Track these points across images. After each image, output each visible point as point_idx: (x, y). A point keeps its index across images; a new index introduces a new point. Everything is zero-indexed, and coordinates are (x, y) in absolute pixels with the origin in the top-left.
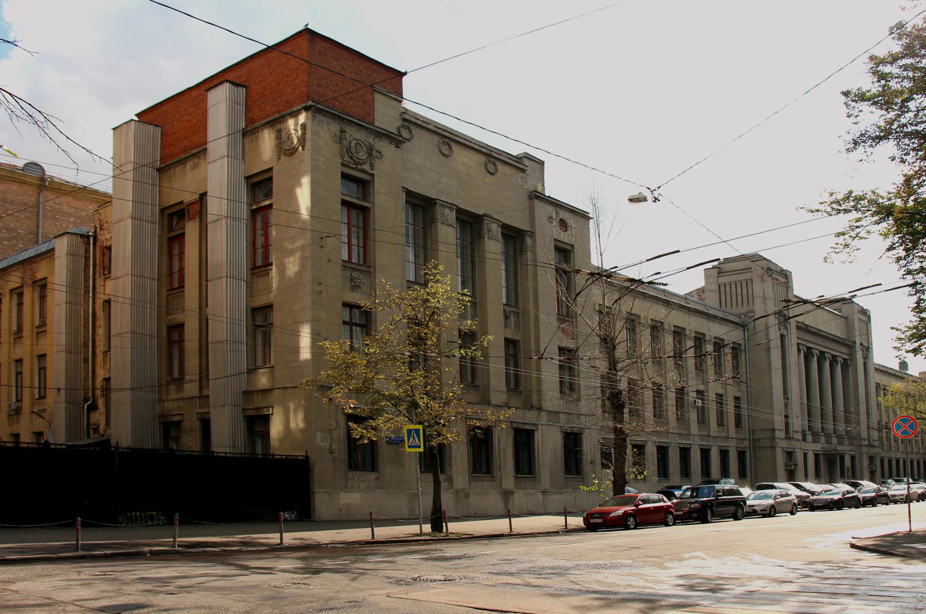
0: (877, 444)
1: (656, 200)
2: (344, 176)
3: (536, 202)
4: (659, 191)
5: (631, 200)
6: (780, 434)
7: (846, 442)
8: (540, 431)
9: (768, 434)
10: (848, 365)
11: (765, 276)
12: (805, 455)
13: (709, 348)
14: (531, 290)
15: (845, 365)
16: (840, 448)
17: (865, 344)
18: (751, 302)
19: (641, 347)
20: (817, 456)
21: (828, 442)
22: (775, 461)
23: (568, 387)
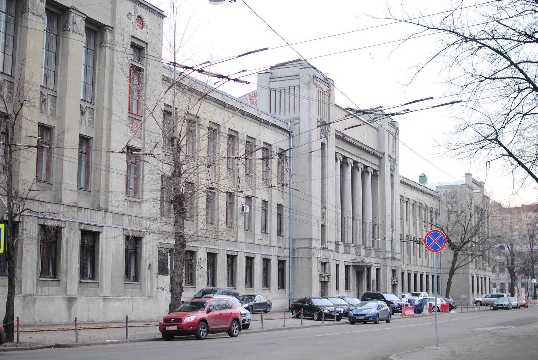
0: (399, 257)
2: (336, 146)
6: (316, 244)
7: (373, 253)
9: (306, 244)
11: (312, 84)
15: (375, 176)
16: (367, 260)
17: (393, 156)
18: (297, 109)
20: (347, 267)
21: (358, 254)
23: (133, 189)
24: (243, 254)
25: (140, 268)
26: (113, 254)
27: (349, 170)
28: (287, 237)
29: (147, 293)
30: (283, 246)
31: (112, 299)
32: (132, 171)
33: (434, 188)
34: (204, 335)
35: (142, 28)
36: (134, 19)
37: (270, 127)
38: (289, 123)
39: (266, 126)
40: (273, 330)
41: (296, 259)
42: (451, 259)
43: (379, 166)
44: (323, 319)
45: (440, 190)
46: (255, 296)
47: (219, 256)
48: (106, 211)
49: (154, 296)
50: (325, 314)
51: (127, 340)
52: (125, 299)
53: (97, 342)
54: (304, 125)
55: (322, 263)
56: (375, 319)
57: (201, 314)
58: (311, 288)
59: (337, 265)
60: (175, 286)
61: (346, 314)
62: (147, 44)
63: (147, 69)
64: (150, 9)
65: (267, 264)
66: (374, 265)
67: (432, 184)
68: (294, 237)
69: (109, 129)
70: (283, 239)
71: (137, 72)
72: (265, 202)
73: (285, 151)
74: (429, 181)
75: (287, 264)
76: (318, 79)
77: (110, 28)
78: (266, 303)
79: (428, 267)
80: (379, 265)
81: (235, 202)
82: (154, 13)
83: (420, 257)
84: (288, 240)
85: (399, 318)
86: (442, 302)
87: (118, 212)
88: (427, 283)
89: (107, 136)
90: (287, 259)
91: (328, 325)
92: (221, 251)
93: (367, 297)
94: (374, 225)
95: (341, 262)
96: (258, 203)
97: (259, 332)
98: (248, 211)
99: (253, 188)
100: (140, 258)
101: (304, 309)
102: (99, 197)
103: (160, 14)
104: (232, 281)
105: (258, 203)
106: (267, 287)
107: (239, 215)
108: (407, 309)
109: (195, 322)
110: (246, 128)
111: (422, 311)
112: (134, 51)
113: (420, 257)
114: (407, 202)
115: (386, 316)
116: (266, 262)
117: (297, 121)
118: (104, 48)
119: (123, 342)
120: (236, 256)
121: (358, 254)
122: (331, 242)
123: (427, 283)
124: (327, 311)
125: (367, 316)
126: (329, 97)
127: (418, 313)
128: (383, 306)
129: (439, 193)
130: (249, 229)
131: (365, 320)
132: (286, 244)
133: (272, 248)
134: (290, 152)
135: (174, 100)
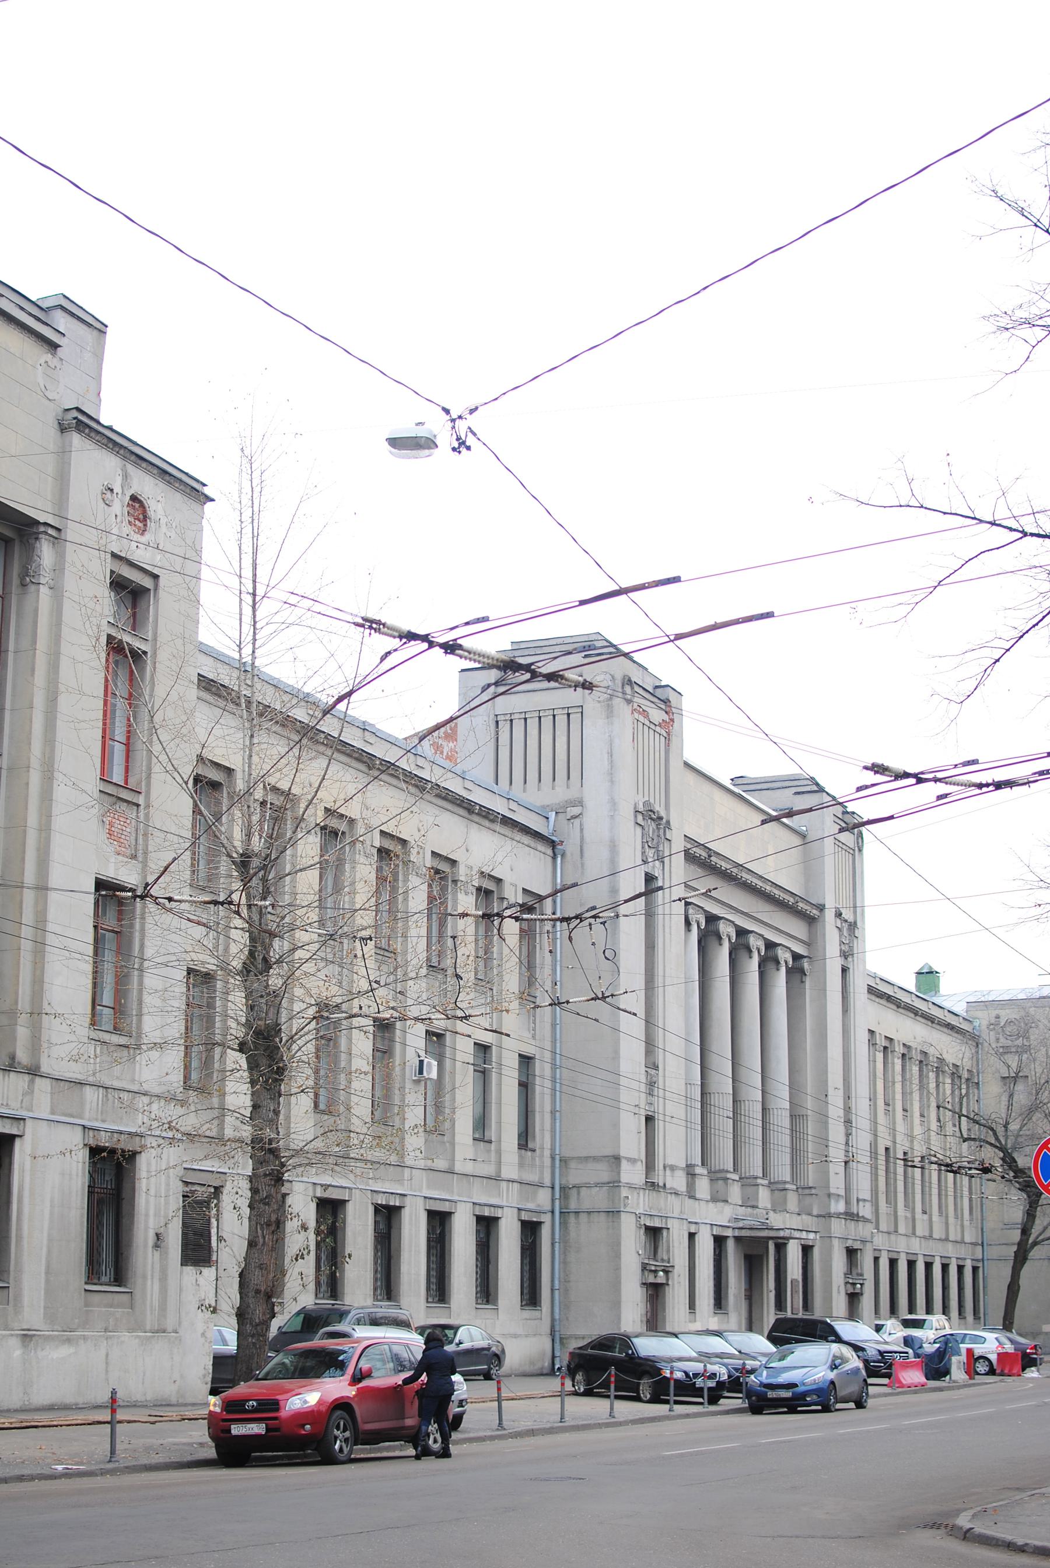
0: (866, 1211)
1: (461, 445)
3: (76, 439)
4: (472, 421)
5: (395, 443)
6: (632, 1174)
7: (792, 1201)
8: (28, 1137)
9: (602, 1173)
10: (803, 972)
11: (618, 702)
12: (876, 1259)
13: (466, 902)
14: (39, 700)
15: (796, 972)
16: (777, 1220)
17: (847, 915)
18: (575, 774)
19: (353, 893)
20: (719, 1241)
21: (749, 1203)
22: (617, 1255)
23: (113, 1009)
24: (420, 1202)
25: (129, 1244)
26: (52, 1201)
27: (723, 954)
28: (547, 1153)
29: (150, 1321)
30: (532, 1177)
31: (47, 1338)
32: (109, 956)
33: (960, 1008)
34: (346, 1450)
35: (143, 532)
36: (119, 506)
37: (498, 827)
38: (552, 815)
39: (487, 823)
40: (532, 1433)
41: (572, 1219)
42: (1017, 1214)
43: (808, 944)
44: (612, 1393)
45: (979, 1014)
46: (455, 1329)
47: (350, 1208)
48: (34, 1072)
49: (170, 1329)
50: (677, 1381)
51: (113, 1464)
52: (85, 1338)
53: (26, 1472)
54: (596, 821)
55: (648, 1229)
56: (821, 1400)
57: (335, 1387)
58: (616, 1305)
59: (692, 1236)
60: (251, 1301)
61: (734, 1384)
62: (156, 577)
63: (155, 653)
64: (167, 474)
65: (488, 1234)
66: (797, 1234)
67: (954, 994)
68: (567, 1154)
69: (45, 829)
70: (533, 1159)
71: (125, 658)
72: (483, 1049)
73: (541, 898)
74: (946, 986)
75: (545, 1232)
76: (637, 689)
77: (50, 531)
78: (488, 1349)
79: (947, 1239)
80: (812, 1236)
81: (398, 1048)
82: (177, 489)
83: (924, 1212)
84: (547, 1162)
85: (886, 1395)
86: (1001, 1344)
87: (68, 1075)
88: (945, 1288)
89: (38, 850)
90: (546, 1218)
91: (687, 1416)
92: (356, 1194)
93: (787, 1333)
94: (796, 1117)
95: (702, 1227)
96: (463, 1050)
97: (492, 1438)
98: (434, 1075)
99: (497, 1008)
100: (132, 1215)
101: (608, 1369)
102: (14, 1031)
103: (194, 492)
104: (387, 1284)
105: (463, 1050)
106: (488, 1302)
107: (409, 1085)
108: (907, 1366)
109: (319, 1412)
110: (432, 830)
111: (947, 1372)
112: (120, 601)
113: (924, 1212)
114: (885, 1048)
115: (853, 1388)
116: (486, 1226)
117: (576, 811)
118: (32, 588)
119: (103, 1473)
120: (399, 1209)
121: (749, 1203)
122: (673, 1168)
123: (945, 1288)
124: (678, 1375)
125: (801, 1389)
126: (668, 739)
127: (934, 1379)
128: (844, 1360)
129: (976, 1024)
130: (437, 1127)
131: (794, 1401)
132: (542, 1173)
133: (504, 1184)
134: (554, 902)
135: (252, 744)
